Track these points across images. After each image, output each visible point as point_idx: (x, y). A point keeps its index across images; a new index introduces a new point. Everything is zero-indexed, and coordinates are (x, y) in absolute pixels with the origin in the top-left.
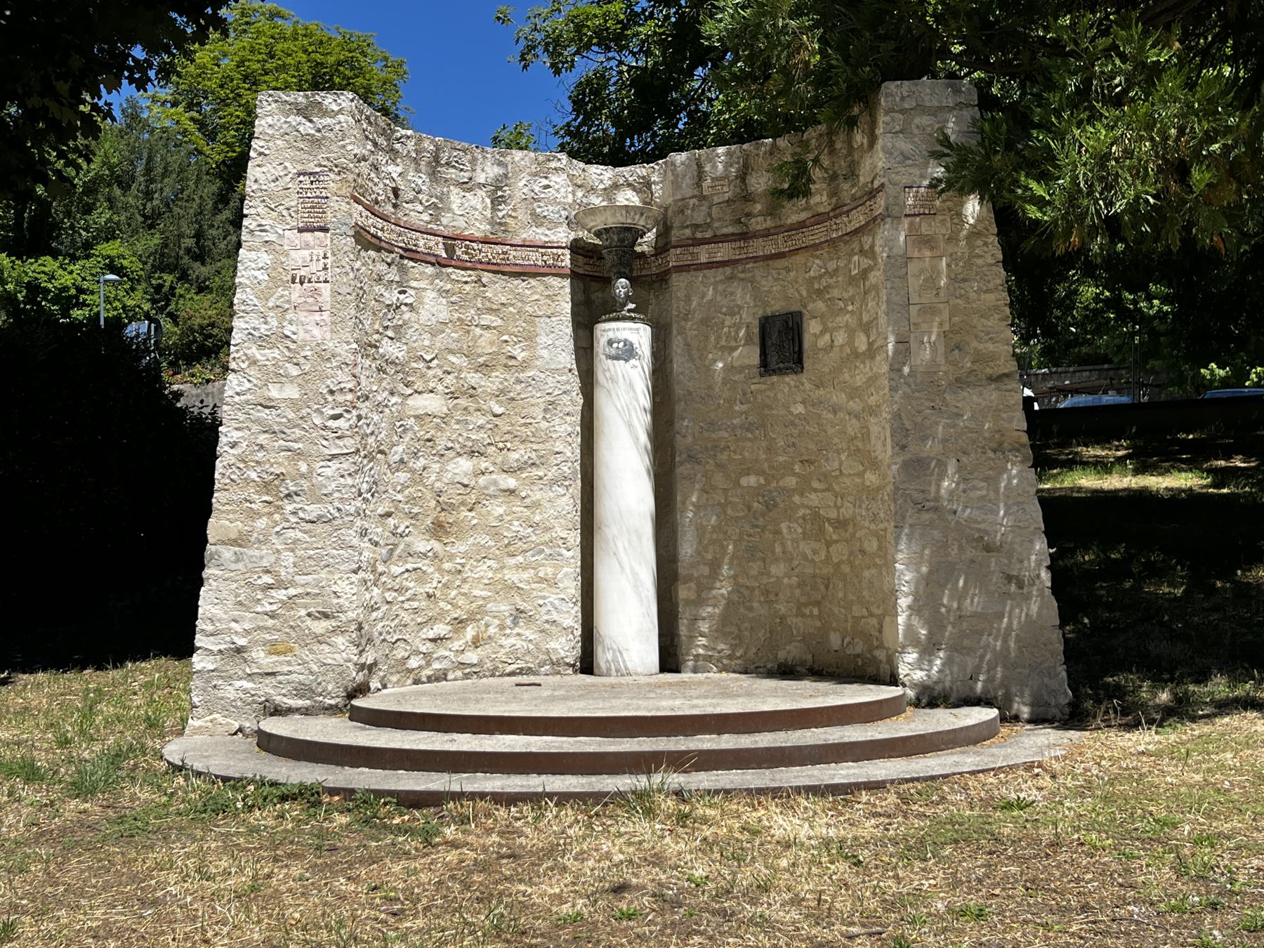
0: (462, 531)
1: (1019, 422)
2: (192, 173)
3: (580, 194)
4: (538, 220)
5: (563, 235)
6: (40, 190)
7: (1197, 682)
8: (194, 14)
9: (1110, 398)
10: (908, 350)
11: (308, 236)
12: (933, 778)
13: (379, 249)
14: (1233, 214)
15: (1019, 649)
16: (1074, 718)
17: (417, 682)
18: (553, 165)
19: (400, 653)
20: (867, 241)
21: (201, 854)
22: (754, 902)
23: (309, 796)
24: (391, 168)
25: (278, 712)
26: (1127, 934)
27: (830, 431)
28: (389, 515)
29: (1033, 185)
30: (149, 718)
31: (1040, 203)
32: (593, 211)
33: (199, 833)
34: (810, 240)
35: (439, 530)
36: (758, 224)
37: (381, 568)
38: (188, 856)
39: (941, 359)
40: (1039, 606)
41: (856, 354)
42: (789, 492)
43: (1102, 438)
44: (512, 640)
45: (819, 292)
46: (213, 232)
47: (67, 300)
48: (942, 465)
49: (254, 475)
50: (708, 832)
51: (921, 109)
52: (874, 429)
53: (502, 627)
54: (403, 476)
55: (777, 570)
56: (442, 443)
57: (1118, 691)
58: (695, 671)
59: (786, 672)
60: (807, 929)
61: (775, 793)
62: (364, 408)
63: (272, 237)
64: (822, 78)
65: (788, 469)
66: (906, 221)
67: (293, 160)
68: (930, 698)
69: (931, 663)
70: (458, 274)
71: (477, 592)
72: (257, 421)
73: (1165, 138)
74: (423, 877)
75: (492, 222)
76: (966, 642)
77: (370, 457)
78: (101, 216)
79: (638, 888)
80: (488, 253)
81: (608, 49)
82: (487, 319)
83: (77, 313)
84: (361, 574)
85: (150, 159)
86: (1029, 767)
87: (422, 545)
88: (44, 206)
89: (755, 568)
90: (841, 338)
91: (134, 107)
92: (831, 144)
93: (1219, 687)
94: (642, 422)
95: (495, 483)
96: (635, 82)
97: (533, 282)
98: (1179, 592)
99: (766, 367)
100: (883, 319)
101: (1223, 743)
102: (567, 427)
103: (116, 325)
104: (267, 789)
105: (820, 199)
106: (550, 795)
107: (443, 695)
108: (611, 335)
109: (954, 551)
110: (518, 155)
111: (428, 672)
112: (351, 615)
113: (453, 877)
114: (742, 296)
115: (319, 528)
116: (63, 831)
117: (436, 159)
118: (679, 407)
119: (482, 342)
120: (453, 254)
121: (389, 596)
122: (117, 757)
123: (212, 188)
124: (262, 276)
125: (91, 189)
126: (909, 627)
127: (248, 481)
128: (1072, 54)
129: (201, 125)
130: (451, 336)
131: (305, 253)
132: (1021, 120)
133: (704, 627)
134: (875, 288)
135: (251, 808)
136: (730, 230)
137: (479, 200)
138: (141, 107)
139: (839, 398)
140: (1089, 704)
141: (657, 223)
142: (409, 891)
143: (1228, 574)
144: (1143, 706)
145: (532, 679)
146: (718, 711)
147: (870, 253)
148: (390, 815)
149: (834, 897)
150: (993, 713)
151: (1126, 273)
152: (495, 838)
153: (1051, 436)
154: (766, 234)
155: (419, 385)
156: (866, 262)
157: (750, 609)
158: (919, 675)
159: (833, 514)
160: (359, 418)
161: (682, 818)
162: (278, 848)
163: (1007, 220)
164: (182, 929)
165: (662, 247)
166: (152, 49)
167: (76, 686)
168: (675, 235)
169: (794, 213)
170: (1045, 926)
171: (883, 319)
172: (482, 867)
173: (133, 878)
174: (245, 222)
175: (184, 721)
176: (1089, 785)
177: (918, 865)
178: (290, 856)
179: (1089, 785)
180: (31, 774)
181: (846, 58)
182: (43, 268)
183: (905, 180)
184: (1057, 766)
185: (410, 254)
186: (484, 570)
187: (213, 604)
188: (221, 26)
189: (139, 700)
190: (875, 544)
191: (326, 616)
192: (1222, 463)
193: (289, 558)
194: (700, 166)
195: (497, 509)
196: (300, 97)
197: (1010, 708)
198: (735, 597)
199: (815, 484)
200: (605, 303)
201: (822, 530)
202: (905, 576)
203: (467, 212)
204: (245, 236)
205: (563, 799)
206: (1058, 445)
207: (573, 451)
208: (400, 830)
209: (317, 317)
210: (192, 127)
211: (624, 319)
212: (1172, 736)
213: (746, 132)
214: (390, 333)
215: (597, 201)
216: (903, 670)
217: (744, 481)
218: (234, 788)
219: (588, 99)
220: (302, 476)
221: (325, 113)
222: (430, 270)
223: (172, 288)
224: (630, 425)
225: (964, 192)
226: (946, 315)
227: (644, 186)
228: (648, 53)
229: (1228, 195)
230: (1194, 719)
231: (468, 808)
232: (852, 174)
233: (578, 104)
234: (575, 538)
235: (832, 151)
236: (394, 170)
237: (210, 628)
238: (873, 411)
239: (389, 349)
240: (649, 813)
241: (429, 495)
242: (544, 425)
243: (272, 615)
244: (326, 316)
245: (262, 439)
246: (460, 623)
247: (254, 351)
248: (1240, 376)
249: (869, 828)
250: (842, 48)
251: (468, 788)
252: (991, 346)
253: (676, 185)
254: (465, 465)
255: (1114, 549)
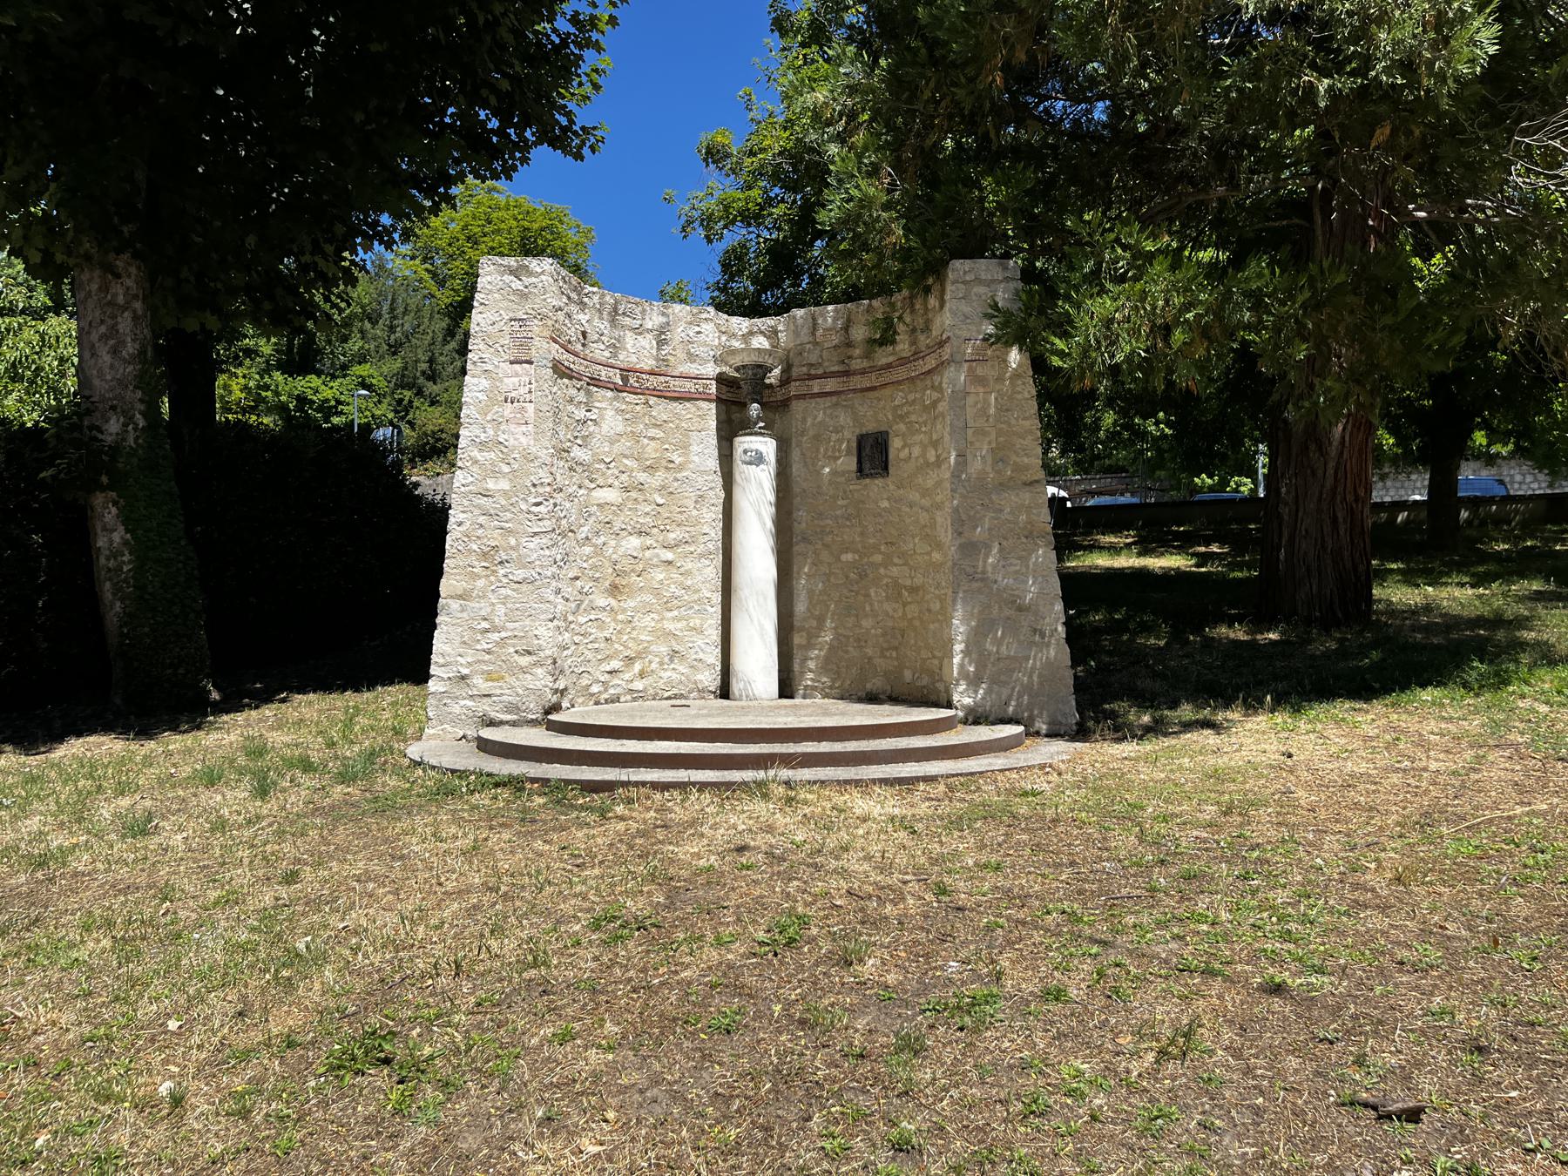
0: (633, 592)
1: (1045, 517)
2: (426, 313)
3: (724, 338)
4: (692, 357)
5: (711, 370)
6: (310, 324)
7: (1170, 708)
8: (430, 192)
9: (1126, 499)
10: (965, 462)
11: (517, 367)
12: (972, 774)
13: (571, 378)
14: (1202, 366)
15: (1041, 683)
16: (1081, 733)
17: (597, 703)
18: (704, 316)
19: (584, 682)
20: (937, 379)
21: (436, 824)
22: (837, 858)
23: (516, 784)
24: (581, 316)
25: (492, 723)
26: (1100, 881)
27: (908, 521)
28: (577, 578)
29: (1057, 341)
30: (394, 728)
31: (1061, 354)
32: (734, 352)
33: (434, 809)
34: (894, 378)
35: (614, 590)
36: (857, 364)
37: (571, 618)
38: (426, 825)
39: (989, 469)
40: (1056, 651)
41: (928, 464)
42: (875, 566)
43: (1115, 529)
44: (669, 673)
45: (901, 417)
46: (442, 358)
47: (328, 410)
48: (988, 547)
49: (475, 547)
50: (807, 811)
51: (978, 281)
52: (939, 520)
53: (661, 664)
54: (588, 550)
55: (867, 623)
56: (617, 525)
57: (1113, 715)
58: (804, 697)
59: (872, 699)
60: (875, 877)
61: (857, 783)
62: (559, 497)
63: (489, 367)
64: (905, 254)
65: (876, 548)
66: (966, 365)
67: (507, 309)
68: (976, 718)
69: (976, 692)
70: (631, 398)
71: (642, 637)
72: (478, 507)
73: (1154, 307)
74: (600, 841)
75: (657, 360)
76: (1003, 678)
77: (563, 535)
78: (355, 344)
79: (754, 848)
80: (654, 381)
81: (749, 225)
82: (653, 432)
83: (336, 420)
84: (556, 622)
85: (393, 300)
86: (1042, 767)
87: (601, 601)
88: (311, 337)
89: (851, 621)
90: (916, 451)
91: (380, 259)
92: (912, 305)
93: (1186, 711)
94: (768, 512)
95: (657, 555)
96: (769, 251)
97: (688, 405)
98: (1162, 643)
99: (861, 472)
100: (947, 438)
101: (1183, 751)
102: (711, 516)
103: (366, 429)
104: (484, 778)
105: (903, 346)
106: (694, 784)
107: (618, 713)
108: (746, 446)
109: (995, 611)
110: (677, 307)
111: (606, 696)
112: (548, 652)
113: (621, 841)
114: (844, 418)
115: (524, 587)
116: (332, 807)
117: (615, 310)
118: (797, 501)
119: (648, 449)
120: (627, 382)
121: (577, 639)
122: (372, 755)
123: (442, 324)
124: (482, 396)
125: (347, 324)
126: (962, 666)
127: (471, 551)
128: (1087, 244)
129: (434, 275)
130: (625, 445)
131: (514, 380)
132: (1051, 294)
133: (812, 664)
134: (942, 415)
135: (472, 792)
136: (835, 368)
137: (648, 342)
138: (391, 265)
139: (914, 496)
140: (1091, 724)
141: (781, 362)
142: (589, 851)
143: (1198, 630)
144: (1130, 726)
145: (683, 702)
146: (813, 725)
147: (939, 389)
148: (575, 798)
149: (895, 855)
150: (1021, 728)
151: (1136, 403)
152: (652, 814)
153: (1071, 526)
154: (863, 372)
155: (600, 481)
156: (936, 395)
157: (847, 652)
158: (968, 701)
159: (908, 582)
160: (555, 505)
161: (789, 800)
162: (491, 820)
163: (1039, 365)
164: (422, 876)
165: (785, 380)
166: (398, 215)
167: (339, 704)
168: (795, 372)
169: (883, 356)
170: (1043, 876)
171: (947, 438)
172: (642, 834)
173: (386, 840)
174: (470, 355)
175: (422, 730)
176: (1085, 780)
177: (956, 834)
178: (502, 825)
179: (1085, 780)
180: (307, 766)
181: (924, 242)
182: (309, 384)
183: (966, 334)
184: (1062, 766)
185: (595, 382)
186: (648, 621)
187: (443, 643)
188: (450, 200)
189: (386, 715)
190: (938, 605)
191: (529, 653)
192: (1202, 549)
193: (501, 610)
194: (814, 319)
195: (659, 575)
196: (512, 262)
197: (1033, 725)
198: (835, 643)
199: (896, 560)
200: (742, 422)
201: (900, 594)
202: (959, 628)
203: (638, 351)
204: (469, 366)
205: (703, 786)
206: (1082, 534)
207: (716, 533)
208: (583, 808)
209: (524, 428)
210: (427, 276)
211: (756, 434)
212: (1147, 747)
213: (851, 295)
214: (579, 441)
215: (737, 344)
216: (956, 698)
217: (844, 557)
218: (460, 778)
219: (733, 263)
220: (512, 548)
221: (531, 274)
222: (610, 394)
223: (411, 402)
224: (759, 514)
225: (1008, 345)
226: (993, 436)
227: (773, 334)
228: (779, 229)
229: (1200, 353)
230: (1166, 735)
231: (633, 792)
232: (927, 329)
233: (726, 266)
234: (717, 598)
235: (913, 311)
236: (583, 318)
237: (441, 661)
238: (939, 507)
239: (578, 453)
240: (766, 796)
241: (607, 564)
242: (695, 513)
243: (489, 652)
244: (530, 427)
245: (482, 519)
246: (630, 660)
247: (476, 454)
248: (1224, 483)
249: (923, 808)
250: (921, 234)
251: (634, 778)
252: (1026, 460)
253: (796, 333)
254: (634, 542)
255: (1117, 611)
